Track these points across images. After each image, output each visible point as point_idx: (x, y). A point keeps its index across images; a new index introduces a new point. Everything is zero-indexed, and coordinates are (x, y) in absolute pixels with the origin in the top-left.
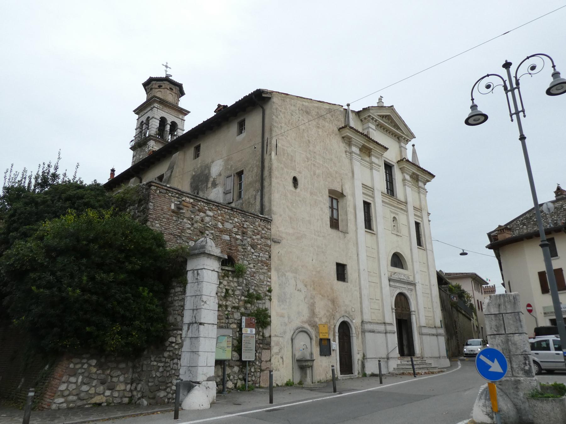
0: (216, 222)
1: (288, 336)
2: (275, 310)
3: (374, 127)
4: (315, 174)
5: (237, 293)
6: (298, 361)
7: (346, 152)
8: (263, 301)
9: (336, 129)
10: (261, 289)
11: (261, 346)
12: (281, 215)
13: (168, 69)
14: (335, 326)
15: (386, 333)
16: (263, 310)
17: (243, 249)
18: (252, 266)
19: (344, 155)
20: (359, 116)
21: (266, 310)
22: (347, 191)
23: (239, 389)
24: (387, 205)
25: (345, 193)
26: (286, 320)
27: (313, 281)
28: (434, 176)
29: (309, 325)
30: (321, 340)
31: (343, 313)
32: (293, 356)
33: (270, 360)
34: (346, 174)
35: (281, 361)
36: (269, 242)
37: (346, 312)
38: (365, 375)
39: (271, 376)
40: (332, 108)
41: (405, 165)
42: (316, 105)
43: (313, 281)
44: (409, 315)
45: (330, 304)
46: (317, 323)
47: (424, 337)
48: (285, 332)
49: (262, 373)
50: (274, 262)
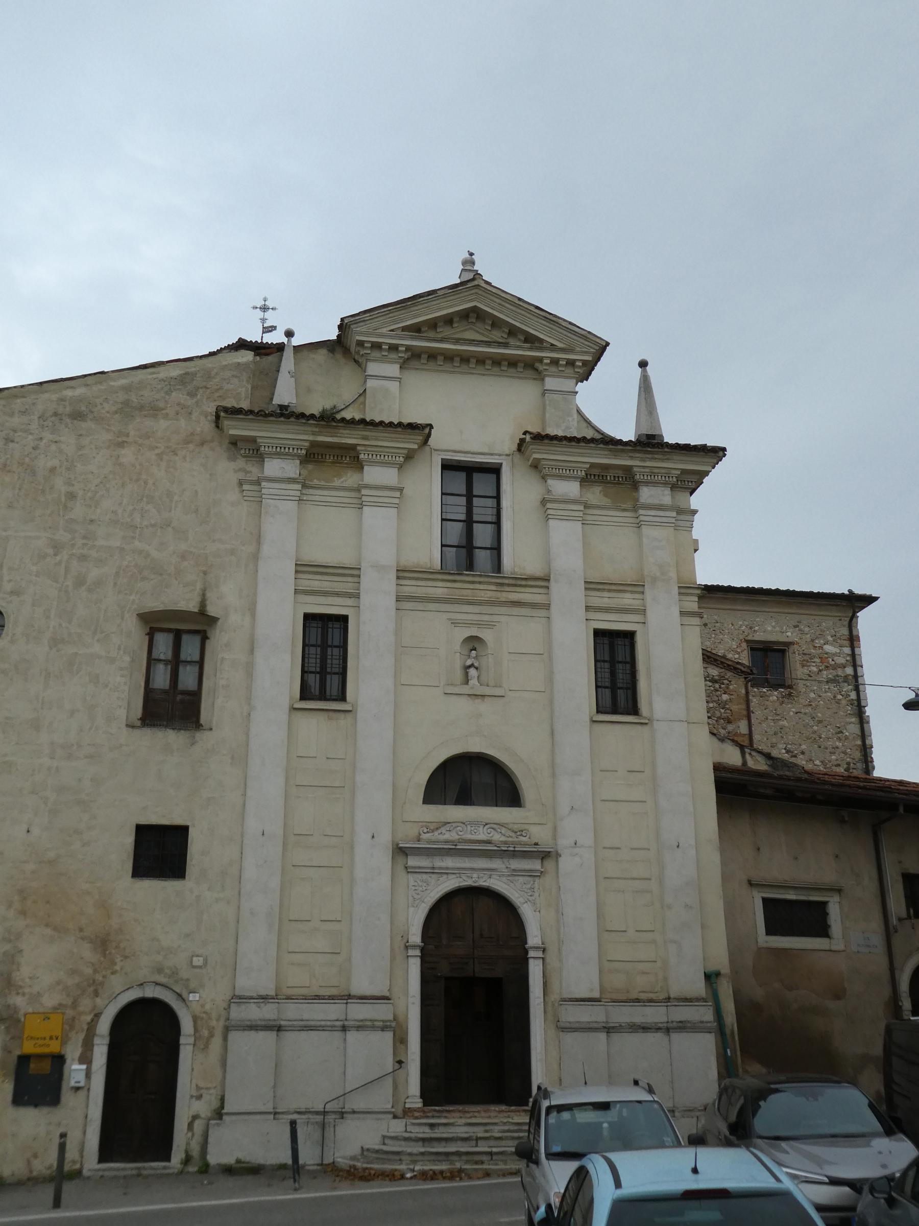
3: (393, 370)
4: (80, 582)
7: (241, 483)
9: (206, 426)
14: (98, 1016)
15: (344, 1029)
19: (233, 495)
20: (346, 351)
22: (225, 600)
24: (432, 606)
25: (212, 611)
27: (21, 892)
28: (724, 449)
30: (24, 1060)
37: (160, 970)
38: (205, 1168)
40: (187, 374)
42: (124, 382)
43: (21, 892)
44: (523, 961)
45: (87, 952)
46: (16, 1009)
47: (569, 1038)
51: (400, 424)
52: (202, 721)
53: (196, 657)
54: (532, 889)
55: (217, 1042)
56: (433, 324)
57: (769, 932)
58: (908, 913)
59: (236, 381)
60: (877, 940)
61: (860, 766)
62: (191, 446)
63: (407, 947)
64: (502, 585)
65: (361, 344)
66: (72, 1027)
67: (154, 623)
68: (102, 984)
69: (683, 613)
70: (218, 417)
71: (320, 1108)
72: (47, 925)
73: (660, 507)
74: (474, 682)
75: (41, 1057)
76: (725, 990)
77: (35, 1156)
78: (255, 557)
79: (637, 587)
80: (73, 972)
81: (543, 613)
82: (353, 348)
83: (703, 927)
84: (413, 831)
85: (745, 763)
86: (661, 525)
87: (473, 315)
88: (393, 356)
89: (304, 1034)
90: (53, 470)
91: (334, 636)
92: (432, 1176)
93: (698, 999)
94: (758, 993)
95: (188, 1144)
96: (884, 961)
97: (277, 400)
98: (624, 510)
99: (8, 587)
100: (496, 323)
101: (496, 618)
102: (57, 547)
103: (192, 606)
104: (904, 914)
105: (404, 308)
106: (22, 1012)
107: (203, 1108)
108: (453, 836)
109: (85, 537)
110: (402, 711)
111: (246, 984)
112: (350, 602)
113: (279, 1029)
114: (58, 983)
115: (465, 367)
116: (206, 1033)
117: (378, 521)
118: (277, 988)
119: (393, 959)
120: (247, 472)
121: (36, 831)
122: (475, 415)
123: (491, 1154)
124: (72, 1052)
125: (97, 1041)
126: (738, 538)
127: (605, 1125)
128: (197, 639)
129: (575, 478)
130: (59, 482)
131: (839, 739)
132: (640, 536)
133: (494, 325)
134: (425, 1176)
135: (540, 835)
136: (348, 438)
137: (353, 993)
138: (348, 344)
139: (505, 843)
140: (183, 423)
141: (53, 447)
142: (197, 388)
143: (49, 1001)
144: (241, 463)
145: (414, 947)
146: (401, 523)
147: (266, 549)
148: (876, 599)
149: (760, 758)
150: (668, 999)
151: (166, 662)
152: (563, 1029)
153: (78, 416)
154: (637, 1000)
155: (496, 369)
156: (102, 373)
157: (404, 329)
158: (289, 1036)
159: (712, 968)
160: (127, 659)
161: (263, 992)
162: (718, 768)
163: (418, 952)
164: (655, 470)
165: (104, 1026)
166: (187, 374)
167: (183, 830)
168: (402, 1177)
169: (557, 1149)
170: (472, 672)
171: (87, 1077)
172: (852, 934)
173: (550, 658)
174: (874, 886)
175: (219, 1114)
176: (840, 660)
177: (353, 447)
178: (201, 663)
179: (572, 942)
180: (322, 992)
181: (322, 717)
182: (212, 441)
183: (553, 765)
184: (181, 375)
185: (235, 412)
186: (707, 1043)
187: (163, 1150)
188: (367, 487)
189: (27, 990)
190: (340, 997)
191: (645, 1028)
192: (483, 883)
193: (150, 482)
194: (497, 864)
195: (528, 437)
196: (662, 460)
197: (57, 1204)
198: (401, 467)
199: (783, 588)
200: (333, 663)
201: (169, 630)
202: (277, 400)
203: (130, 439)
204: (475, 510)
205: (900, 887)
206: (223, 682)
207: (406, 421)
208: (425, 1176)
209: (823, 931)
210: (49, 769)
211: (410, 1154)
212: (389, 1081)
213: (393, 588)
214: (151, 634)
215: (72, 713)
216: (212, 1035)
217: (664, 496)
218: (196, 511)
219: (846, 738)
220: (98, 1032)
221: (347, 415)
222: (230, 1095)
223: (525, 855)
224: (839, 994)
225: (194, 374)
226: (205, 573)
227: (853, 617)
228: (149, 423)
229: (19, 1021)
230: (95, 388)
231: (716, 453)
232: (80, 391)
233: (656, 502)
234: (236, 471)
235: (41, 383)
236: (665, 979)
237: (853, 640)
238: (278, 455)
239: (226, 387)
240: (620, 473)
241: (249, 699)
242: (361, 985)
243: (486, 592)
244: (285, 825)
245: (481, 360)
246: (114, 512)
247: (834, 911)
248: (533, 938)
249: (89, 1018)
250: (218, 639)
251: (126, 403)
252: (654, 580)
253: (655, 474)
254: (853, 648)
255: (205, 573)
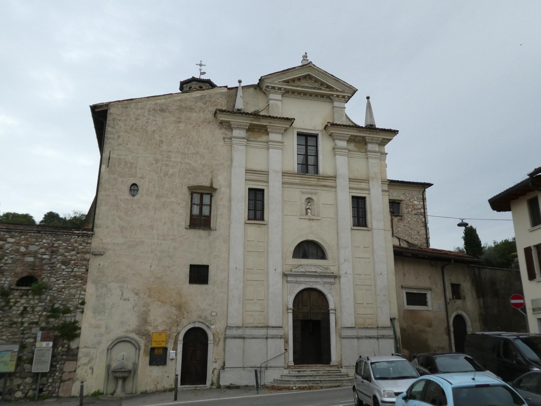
0: (17, 247)
1: (105, 345)
2: (88, 323)
3: (279, 97)
5: (38, 309)
6: (114, 372)
7: (224, 139)
8: (73, 314)
9: (210, 116)
10: (72, 303)
11: (64, 357)
12: (107, 227)
13: (202, 67)
14: (178, 333)
15: (267, 338)
16: (70, 323)
17: (50, 267)
18: (60, 282)
19: (221, 143)
20: (261, 89)
21: (76, 322)
22: (220, 182)
23: (29, 398)
25: (215, 186)
26: (103, 330)
27: (149, 289)
28: (398, 131)
29: (137, 334)
30: (153, 349)
31: (194, 318)
32: (108, 367)
33: (75, 371)
34: (222, 164)
35: (90, 371)
36: (87, 256)
37: (200, 317)
38: (219, 387)
39: (82, 387)
41: (332, 130)
42: (178, 98)
44: (328, 314)
45: (174, 311)
46: (149, 331)
47: (345, 341)
48: (99, 343)
49: (62, 384)
50: (90, 277)
51: (283, 118)
52: (211, 227)
53: (209, 203)
54: (331, 289)
55: (221, 343)
56: (293, 80)
57: (408, 304)
58: (453, 297)
59: (221, 99)
60: (443, 307)
61: (425, 245)
62: (205, 124)
63: (288, 309)
64: (319, 179)
65: (267, 87)
66: (169, 338)
67: (194, 190)
68: (180, 322)
69: (383, 191)
70: (216, 113)
71: (259, 365)
72: (159, 301)
73: (375, 152)
74: (309, 214)
75: (159, 348)
76: (397, 324)
77: (158, 383)
78: (230, 166)
79: (367, 181)
80: (169, 318)
81: (334, 189)
82: (264, 88)
83: (390, 302)
84: (289, 268)
85: (400, 245)
86: (376, 158)
87: (308, 77)
88: (279, 92)
89: (252, 340)
90: (154, 131)
91: (259, 196)
92: (304, 388)
93: (388, 327)
94: (405, 326)
95: (212, 378)
96: (444, 314)
97: (236, 107)
98: (362, 152)
99: (139, 175)
100: (316, 80)
101: (317, 191)
102: (157, 161)
103: (208, 184)
104: (451, 298)
105: (283, 74)
106: (151, 332)
107: (218, 366)
108: (303, 270)
109: (167, 157)
110: (285, 224)
111: (231, 322)
112: (265, 184)
113: (244, 338)
114: (164, 322)
115: (305, 97)
116: (217, 339)
117: (275, 154)
118: (243, 324)
119: (283, 313)
120: (226, 134)
121: (153, 267)
122: (309, 115)
123: (321, 381)
124: (170, 346)
125: (179, 342)
126: (400, 163)
127: (391, 369)
128: (209, 196)
129: (345, 140)
130: (156, 136)
131: (418, 235)
132: (368, 162)
133: (315, 81)
134: (300, 388)
135: (333, 269)
136: (264, 122)
137: (269, 325)
138: (261, 87)
139: (322, 272)
140: (202, 114)
141: (154, 122)
142: (207, 101)
143: (161, 328)
144: (223, 130)
145: (290, 309)
146: (282, 156)
147: (234, 164)
148: (432, 185)
149: (405, 243)
150: (378, 327)
151: (198, 205)
152: (343, 338)
153: (162, 110)
154: (367, 328)
155: (316, 98)
156: (171, 94)
157: (283, 81)
158: (247, 341)
159: (393, 317)
160: (185, 203)
161: (238, 325)
162: (394, 247)
163: (292, 311)
164: (371, 137)
165: (181, 337)
166: (203, 95)
167: (207, 267)
168: (292, 389)
169: (378, 376)
170: (309, 211)
171: (175, 355)
172: (435, 304)
173: (337, 207)
174: (442, 288)
175: (223, 367)
176: (419, 207)
177: (266, 126)
178: (210, 205)
179: (345, 308)
180: (259, 325)
181: (256, 226)
182: (213, 122)
183: (338, 244)
184: (200, 96)
185: (222, 111)
186: (392, 342)
187: (203, 380)
188: (270, 141)
189: (153, 324)
190: (265, 327)
191: (370, 338)
192: (314, 286)
193: (191, 137)
194: (318, 280)
195: (329, 125)
196: (376, 134)
197: (176, 399)
198: (282, 134)
199: (400, 180)
200: (259, 207)
201: (198, 193)
202: (236, 107)
203: (182, 120)
204: (309, 151)
205: (450, 288)
206: (219, 213)
207: (285, 116)
208: (300, 388)
209: (425, 303)
210: (157, 244)
211: (293, 381)
212: (283, 356)
213: (281, 179)
214: (192, 194)
215: (165, 223)
216: (220, 340)
217: (376, 148)
218: (208, 148)
219: (421, 235)
220: (179, 339)
221: (261, 114)
222: (227, 361)
223: (329, 277)
224: (430, 326)
225: (205, 96)
226: (212, 172)
227: (424, 191)
228: (189, 114)
229: (150, 335)
230: (169, 100)
231: (395, 132)
232: (163, 101)
233: (373, 150)
234: (222, 134)
235: (148, 97)
236: (377, 320)
237: (424, 199)
238: (238, 128)
239: (218, 101)
240: (361, 139)
241: (229, 219)
242: (272, 323)
243: (314, 181)
244: (244, 266)
245: (311, 94)
246: (178, 148)
247: (429, 297)
248: (331, 306)
249: (175, 334)
250: (217, 197)
251: (180, 106)
252: (373, 178)
253: (373, 139)
254: (424, 202)
255: (212, 172)
